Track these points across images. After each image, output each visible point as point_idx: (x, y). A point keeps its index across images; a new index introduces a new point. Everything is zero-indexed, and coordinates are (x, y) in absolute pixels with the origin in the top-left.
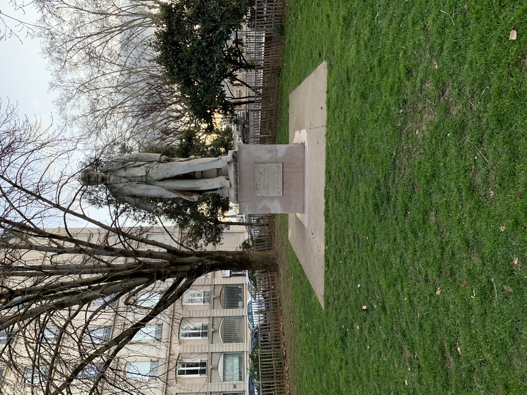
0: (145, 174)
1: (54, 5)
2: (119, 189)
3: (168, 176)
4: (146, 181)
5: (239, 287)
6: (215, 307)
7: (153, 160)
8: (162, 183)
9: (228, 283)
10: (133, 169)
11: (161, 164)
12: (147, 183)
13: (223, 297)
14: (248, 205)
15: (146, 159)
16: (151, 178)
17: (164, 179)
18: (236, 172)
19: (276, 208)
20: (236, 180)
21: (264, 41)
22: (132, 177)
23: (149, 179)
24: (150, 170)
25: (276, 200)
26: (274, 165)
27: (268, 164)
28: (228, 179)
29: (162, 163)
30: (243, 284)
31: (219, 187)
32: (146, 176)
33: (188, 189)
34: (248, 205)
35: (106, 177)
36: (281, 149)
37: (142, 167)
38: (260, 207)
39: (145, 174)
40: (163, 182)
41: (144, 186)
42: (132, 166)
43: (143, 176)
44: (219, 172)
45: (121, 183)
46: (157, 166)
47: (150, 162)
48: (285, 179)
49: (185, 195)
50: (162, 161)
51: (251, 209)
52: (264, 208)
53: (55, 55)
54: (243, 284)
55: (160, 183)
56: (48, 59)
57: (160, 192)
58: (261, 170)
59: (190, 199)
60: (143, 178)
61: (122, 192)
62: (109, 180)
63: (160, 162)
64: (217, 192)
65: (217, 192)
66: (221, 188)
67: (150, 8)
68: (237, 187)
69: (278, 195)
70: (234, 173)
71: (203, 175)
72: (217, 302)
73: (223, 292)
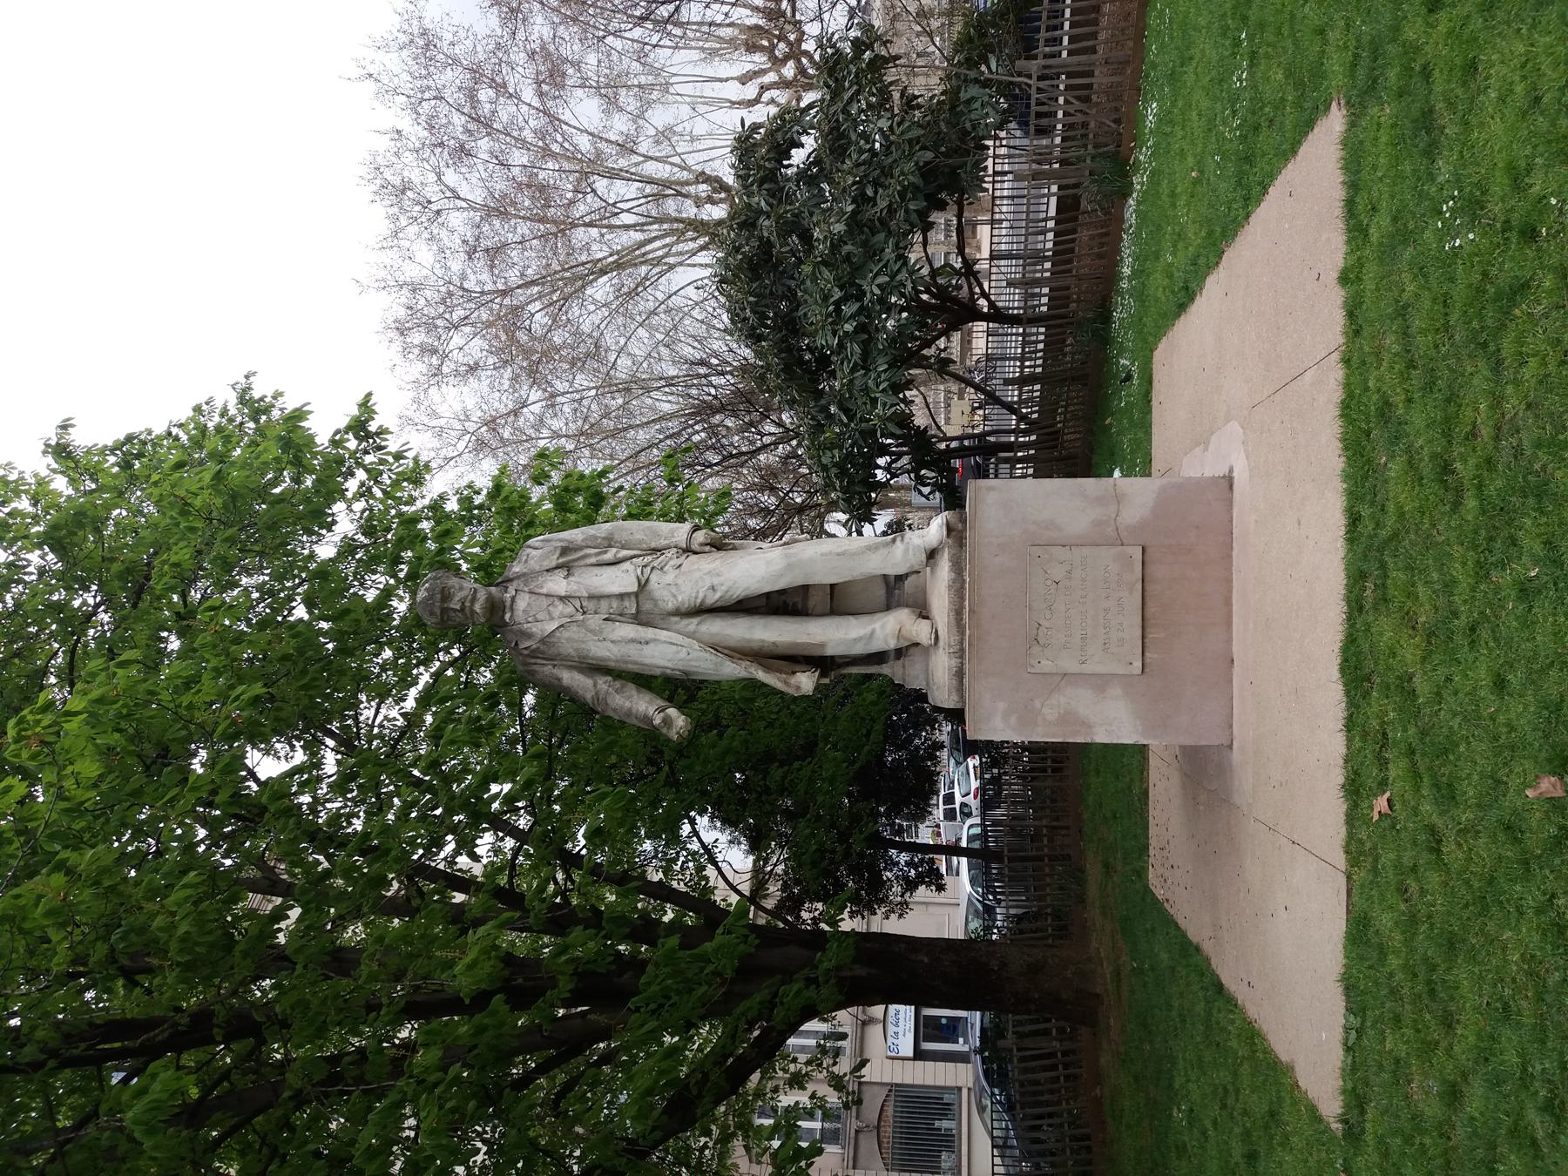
0: (635, 588)
1: (430, 202)
2: (543, 641)
3: (712, 599)
4: (640, 609)
5: (947, 1098)
6: (861, 1161)
7: (664, 542)
8: (692, 624)
9: (908, 1081)
10: (597, 570)
11: (693, 558)
12: (639, 619)
13: (888, 1131)
14: (1001, 706)
15: (641, 541)
16: (655, 601)
17: (702, 611)
18: (958, 588)
19: (1112, 723)
20: (958, 613)
21: (1052, 212)
22: (591, 597)
23: (647, 606)
24: (654, 578)
25: (1116, 691)
26: (1107, 555)
27: (1084, 549)
28: (927, 618)
29: (696, 553)
30: (960, 1089)
31: (892, 644)
32: (636, 594)
33: (780, 651)
34: (1001, 706)
35: (503, 602)
36: (1129, 496)
37: (626, 565)
38: (1050, 713)
39: (635, 588)
40: (695, 621)
41: (627, 631)
42: (593, 560)
43: (628, 594)
44: (895, 591)
45: (552, 619)
46: (679, 562)
47: (655, 550)
48: (1152, 608)
49: (768, 669)
50: (695, 547)
51: (1013, 720)
52: (1067, 718)
53: (417, 337)
54: (960, 1089)
55: (685, 621)
56: (397, 346)
57: (683, 654)
58: (1058, 572)
59: (787, 683)
60: (627, 603)
61: (553, 651)
62: (512, 609)
63: (688, 550)
64: (885, 669)
65: (885, 669)
66: (900, 653)
67: (699, 203)
68: (961, 642)
69: (1121, 670)
70: (950, 587)
71: (836, 600)
72: (869, 1143)
73: (890, 1111)
